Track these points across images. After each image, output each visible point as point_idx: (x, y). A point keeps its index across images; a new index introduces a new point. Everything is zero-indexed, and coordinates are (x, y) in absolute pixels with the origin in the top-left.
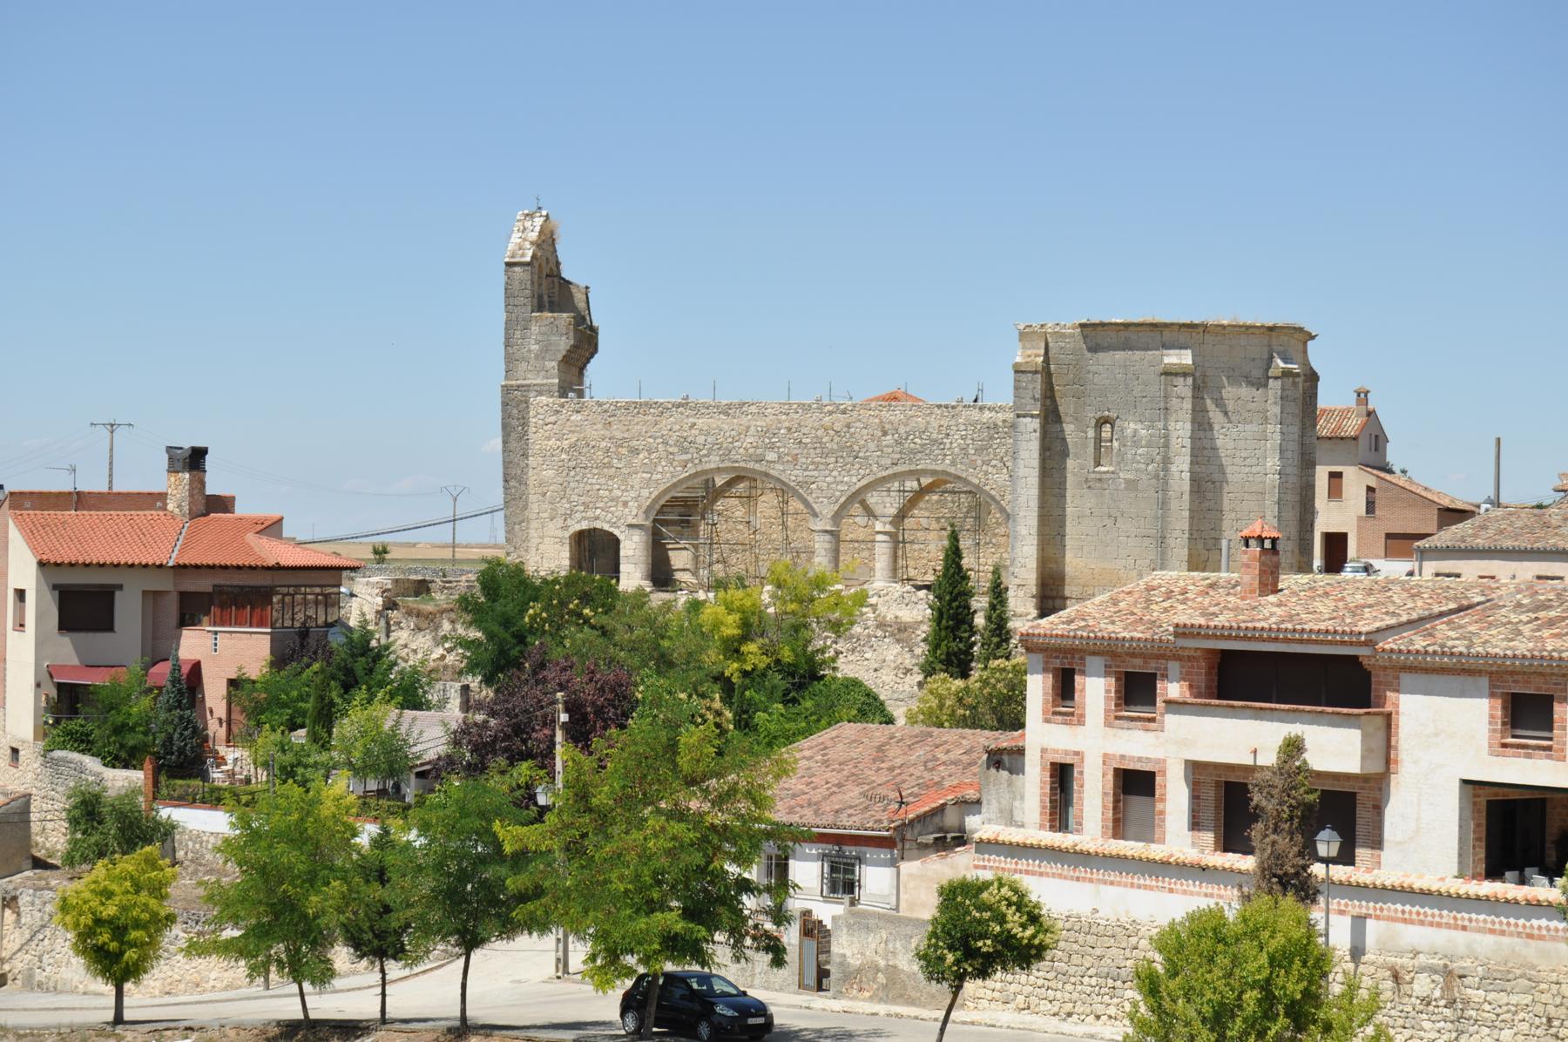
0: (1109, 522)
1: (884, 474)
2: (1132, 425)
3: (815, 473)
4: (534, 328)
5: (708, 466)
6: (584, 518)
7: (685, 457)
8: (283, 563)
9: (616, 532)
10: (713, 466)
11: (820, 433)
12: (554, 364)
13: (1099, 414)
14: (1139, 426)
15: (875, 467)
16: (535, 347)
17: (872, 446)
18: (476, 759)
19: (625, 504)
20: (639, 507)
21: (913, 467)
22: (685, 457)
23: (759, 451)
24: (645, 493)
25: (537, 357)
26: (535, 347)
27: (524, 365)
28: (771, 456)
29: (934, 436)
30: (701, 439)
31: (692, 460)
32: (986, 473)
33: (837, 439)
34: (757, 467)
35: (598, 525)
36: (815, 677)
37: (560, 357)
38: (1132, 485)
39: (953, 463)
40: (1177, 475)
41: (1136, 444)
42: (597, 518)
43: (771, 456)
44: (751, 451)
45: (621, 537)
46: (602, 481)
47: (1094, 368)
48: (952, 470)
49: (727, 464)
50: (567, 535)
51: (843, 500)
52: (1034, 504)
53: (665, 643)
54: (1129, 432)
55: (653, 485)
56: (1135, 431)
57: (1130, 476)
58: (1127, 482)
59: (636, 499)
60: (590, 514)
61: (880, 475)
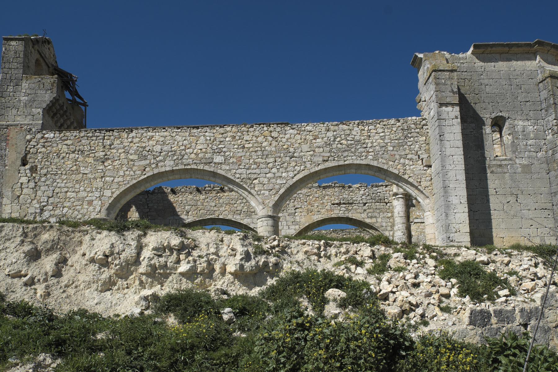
0: (512, 199)
1: (317, 169)
2: (521, 123)
3: (257, 171)
4: (25, 85)
5: (163, 170)
7: (144, 163)
10: (168, 169)
12: (40, 110)
14: (526, 123)
16: (24, 98)
17: (305, 147)
18: (50, 331)
19: (90, 203)
20: (102, 206)
21: (341, 163)
22: (144, 163)
23: (208, 156)
24: (108, 193)
26: (24, 98)
27: (14, 111)
28: (218, 159)
29: (357, 138)
31: (150, 165)
32: (404, 165)
33: (274, 143)
34: (207, 168)
36: (399, 346)
37: (44, 105)
38: (527, 169)
39: (375, 159)
41: (526, 137)
43: (218, 159)
44: (201, 155)
47: (486, 81)
48: (375, 163)
49: (181, 167)
51: (282, 191)
53: (247, 317)
55: (115, 186)
57: (525, 162)
58: (523, 166)
59: (100, 198)
61: (313, 170)
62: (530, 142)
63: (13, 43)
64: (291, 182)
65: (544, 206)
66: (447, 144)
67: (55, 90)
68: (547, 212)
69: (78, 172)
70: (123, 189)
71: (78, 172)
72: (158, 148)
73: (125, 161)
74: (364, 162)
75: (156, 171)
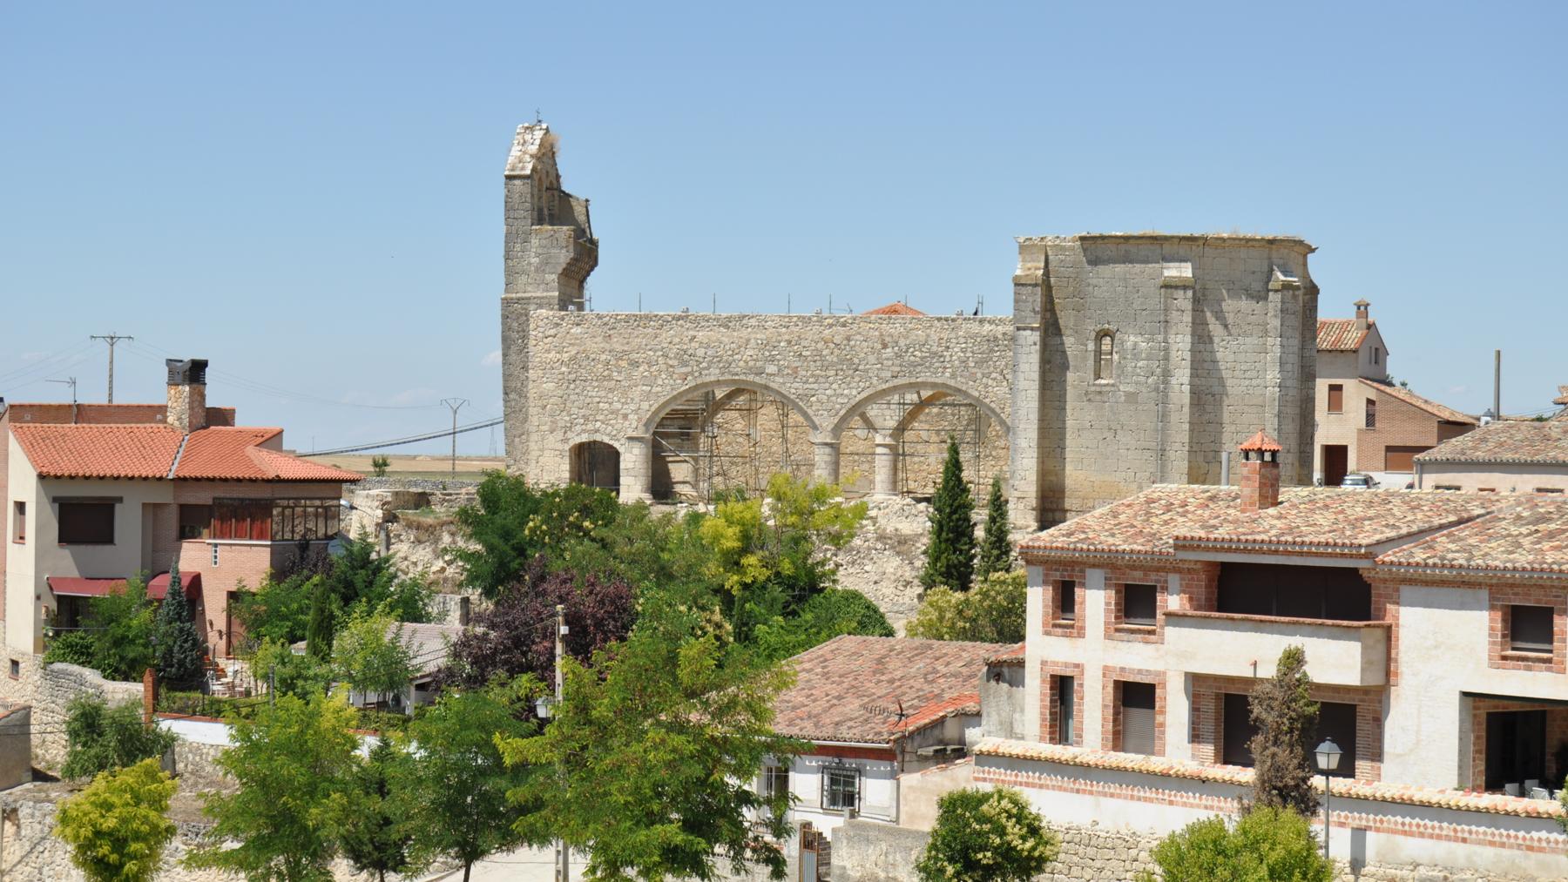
0: (1109, 435)
1: (884, 386)
2: (1132, 338)
3: (815, 386)
4: (535, 241)
5: (708, 379)
6: (584, 431)
7: (684, 370)
8: (283, 476)
9: (616, 445)
10: (713, 378)
11: (820, 346)
12: (554, 277)
13: (1099, 327)
14: (1139, 339)
15: (875, 380)
16: (535, 260)
17: (872, 359)
18: (476, 671)
19: (625, 417)
20: (640, 419)
21: (913, 380)
22: (684, 370)
24: (645, 406)
25: (537, 270)
26: (535, 260)
27: (524, 278)
28: (771, 369)
29: (934, 349)
30: (701, 352)
31: (692, 373)
32: (986, 386)
34: (757, 379)
35: (598, 437)
36: (815, 589)
37: (560, 270)
38: (1132, 398)
39: (953, 376)
40: (1177, 387)
41: (1136, 357)
42: (597, 431)
43: (771, 369)
44: (751, 364)
45: (621, 450)
46: (603, 393)
47: (1094, 281)
48: (952, 383)
49: (727, 377)
50: (567, 447)
51: (843, 412)
52: (1034, 417)
53: (665, 556)
54: (1129, 345)
56: (1136, 344)
57: (1130, 389)
58: (1128, 394)
60: (590, 427)
62: (1140, 364)
63: (517, 182)
64: (853, 402)
65: (1147, 445)
66: (1021, 376)
67: (571, 248)
68: (1148, 453)
69: (609, 378)
70: (662, 400)
71: (609, 378)
72: (701, 352)
73: (664, 367)
74: (939, 381)
75: (699, 381)
